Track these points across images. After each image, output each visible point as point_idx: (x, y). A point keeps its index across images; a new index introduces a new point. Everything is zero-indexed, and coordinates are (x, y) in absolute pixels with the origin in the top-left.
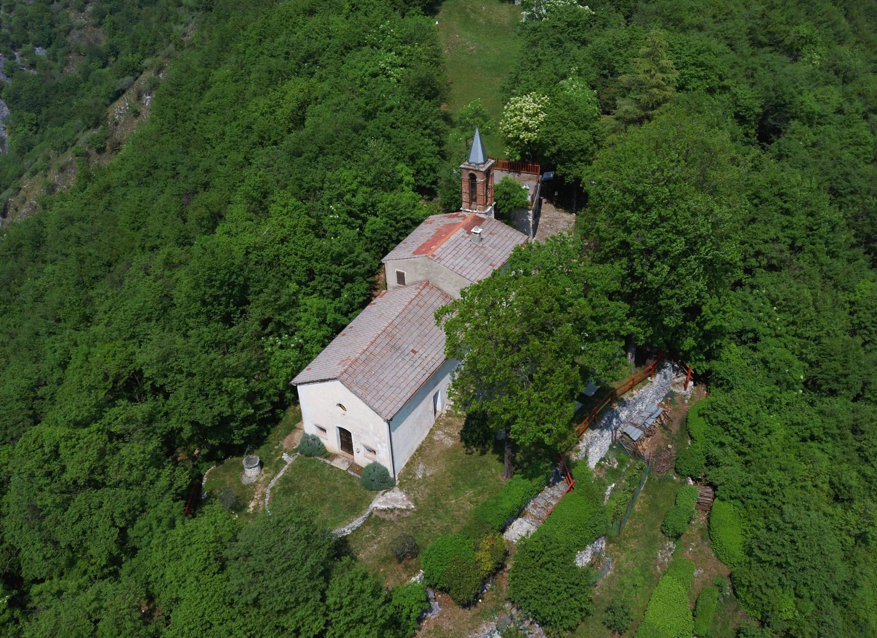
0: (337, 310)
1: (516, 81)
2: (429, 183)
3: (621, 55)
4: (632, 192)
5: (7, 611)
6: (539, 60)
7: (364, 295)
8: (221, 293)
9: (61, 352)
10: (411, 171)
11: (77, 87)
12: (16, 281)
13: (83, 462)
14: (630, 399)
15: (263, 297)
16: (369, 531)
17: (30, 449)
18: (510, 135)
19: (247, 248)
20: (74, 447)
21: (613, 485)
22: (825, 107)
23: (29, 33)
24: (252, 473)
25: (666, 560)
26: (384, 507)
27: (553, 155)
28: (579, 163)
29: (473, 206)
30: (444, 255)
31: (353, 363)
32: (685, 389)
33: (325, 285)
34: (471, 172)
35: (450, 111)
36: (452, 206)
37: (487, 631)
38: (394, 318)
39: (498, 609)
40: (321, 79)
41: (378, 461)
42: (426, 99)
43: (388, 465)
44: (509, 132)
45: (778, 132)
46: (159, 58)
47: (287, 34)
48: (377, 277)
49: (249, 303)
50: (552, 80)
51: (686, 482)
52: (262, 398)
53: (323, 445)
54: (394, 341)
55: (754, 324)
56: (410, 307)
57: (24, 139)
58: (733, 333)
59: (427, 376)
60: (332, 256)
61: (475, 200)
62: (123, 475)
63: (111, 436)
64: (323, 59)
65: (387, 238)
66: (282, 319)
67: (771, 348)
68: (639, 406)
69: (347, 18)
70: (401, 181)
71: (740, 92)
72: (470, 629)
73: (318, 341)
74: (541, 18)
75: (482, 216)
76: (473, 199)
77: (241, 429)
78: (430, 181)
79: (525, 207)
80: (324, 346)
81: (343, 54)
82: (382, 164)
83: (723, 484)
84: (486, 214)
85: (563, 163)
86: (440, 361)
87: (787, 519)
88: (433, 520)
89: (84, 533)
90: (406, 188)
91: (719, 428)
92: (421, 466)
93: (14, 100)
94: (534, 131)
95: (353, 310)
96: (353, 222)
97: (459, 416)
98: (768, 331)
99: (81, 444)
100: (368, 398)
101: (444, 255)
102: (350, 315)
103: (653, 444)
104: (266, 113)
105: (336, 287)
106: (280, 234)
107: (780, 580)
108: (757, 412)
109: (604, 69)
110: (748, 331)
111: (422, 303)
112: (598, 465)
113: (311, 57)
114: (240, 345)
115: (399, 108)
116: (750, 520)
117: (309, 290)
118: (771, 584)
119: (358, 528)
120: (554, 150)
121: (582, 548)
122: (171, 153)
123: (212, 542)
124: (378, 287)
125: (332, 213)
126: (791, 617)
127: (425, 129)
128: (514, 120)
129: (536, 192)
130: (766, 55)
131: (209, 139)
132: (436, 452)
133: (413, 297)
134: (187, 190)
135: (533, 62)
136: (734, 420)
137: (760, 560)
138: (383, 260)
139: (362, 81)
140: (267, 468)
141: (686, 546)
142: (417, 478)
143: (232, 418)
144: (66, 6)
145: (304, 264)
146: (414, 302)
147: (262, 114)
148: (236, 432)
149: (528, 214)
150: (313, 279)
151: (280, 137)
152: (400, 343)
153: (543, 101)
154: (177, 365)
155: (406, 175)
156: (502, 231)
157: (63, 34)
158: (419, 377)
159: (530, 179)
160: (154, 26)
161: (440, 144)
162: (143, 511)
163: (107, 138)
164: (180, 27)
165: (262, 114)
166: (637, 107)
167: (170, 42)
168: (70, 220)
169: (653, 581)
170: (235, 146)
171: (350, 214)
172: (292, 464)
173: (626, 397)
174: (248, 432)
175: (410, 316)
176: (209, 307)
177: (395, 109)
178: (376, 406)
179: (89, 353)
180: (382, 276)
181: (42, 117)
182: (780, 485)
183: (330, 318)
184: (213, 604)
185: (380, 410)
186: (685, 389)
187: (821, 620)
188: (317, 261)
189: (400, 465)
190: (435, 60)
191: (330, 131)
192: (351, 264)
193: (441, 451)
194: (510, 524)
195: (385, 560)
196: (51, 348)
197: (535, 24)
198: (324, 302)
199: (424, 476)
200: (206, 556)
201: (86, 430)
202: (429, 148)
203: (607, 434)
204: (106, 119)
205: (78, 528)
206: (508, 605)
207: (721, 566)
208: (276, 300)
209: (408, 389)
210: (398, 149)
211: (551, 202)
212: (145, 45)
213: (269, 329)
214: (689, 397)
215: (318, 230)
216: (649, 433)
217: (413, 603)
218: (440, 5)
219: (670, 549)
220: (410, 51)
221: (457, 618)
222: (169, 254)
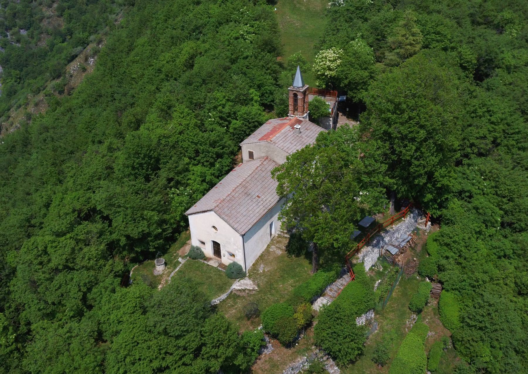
0: (213, 174)
1: (324, 42)
2: (269, 102)
3: (389, 27)
4: (391, 102)
5: (14, 344)
6: (338, 29)
7: (229, 166)
8: (143, 162)
9: (46, 197)
10: (258, 94)
11: (46, 54)
12: (12, 166)
13: (62, 255)
14: (391, 230)
15: (168, 165)
16: (230, 302)
17: (30, 249)
18: (319, 73)
19: (159, 137)
20: (56, 247)
21: (380, 281)
22: (519, 61)
23: (16, 20)
24: (160, 269)
25: (412, 325)
27: (346, 86)
28: (361, 90)
29: (295, 113)
30: (278, 141)
31: (222, 201)
32: (426, 226)
33: (205, 159)
34: (294, 92)
35: (283, 62)
36: (283, 114)
37: (301, 362)
38: (247, 177)
39: (308, 349)
40: (204, 42)
41: (236, 261)
42: (268, 52)
43: (241, 263)
44: (318, 71)
45: (487, 76)
46: (100, 35)
47: (183, 16)
48: (236, 157)
49: (160, 169)
50: (345, 40)
51: (425, 280)
52: (166, 225)
53: (203, 253)
54: (246, 190)
55: (469, 187)
56: (257, 171)
57: (11, 87)
58: (456, 193)
59: (266, 211)
60: (210, 142)
61: (297, 110)
62: (85, 263)
63: (78, 241)
64: (205, 31)
65: (243, 133)
66: (180, 179)
67: (480, 201)
68: (396, 235)
69: (220, 6)
70: (252, 99)
71: (463, 50)
72: (290, 360)
73: (201, 192)
74: (340, 6)
75: (301, 119)
76: (295, 109)
77: (153, 242)
78: (270, 100)
79: (327, 116)
80: (204, 195)
81: (217, 27)
82: (241, 89)
83: (447, 281)
84: (303, 118)
85: (351, 90)
86: (274, 203)
87: (485, 300)
88: (269, 296)
89: (62, 295)
90: (255, 104)
91: (445, 248)
92: (262, 266)
93: (6, 62)
94: (334, 70)
95: (222, 175)
96: (223, 123)
97: (286, 237)
98: (478, 191)
99: (61, 245)
100: (231, 222)
101: (278, 141)
102: (220, 178)
103: (405, 258)
104: (170, 61)
105: (212, 160)
106: (180, 128)
107: (481, 337)
108: (469, 238)
109: (378, 35)
110: (466, 192)
111: (263, 169)
112: (370, 269)
113: (197, 28)
114: (154, 192)
115: (251, 57)
116: (463, 302)
117: (196, 162)
118: (475, 339)
119: (224, 300)
120: (346, 82)
121: (360, 315)
122: (111, 87)
123: (138, 298)
124: (237, 162)
125: (210, 117)
126: (488, 360)
127: (267, 70)
128: (322, 63)
129: (334, 107)
130: (481, 29)
131: (134, 78)
132: (271, 257)
133: (258, 165)
134: (121, 108)
135: (334, 30)
136: (454, 242)
137: (468, 325)
138: (241, 145)
139: (229, 42)
140: (169, 266)
141: (424, 318)
142: (259, 272)
143: (149, 234)
144: (40, 4)
145: (193, 146)
146: (259, 168)
147: (167, 62)
148: (151, 243)
149: (330, 120)
150: (198, 156)
151: (178, 76)
152: (250, 191)
153: (339, 53)
154: (118, 203)
155: (255, 96)
156: (313, 128)
157: (38, 21)
158: (261, 211)
159: (331, 100)
160: (97, 16)
161: (276, 79)
162: (96, 284)
163: (65, 85)
164: (114, 16)
165: (167, 62)
166: (398, 58)
167: (107, 25)
168: (47, 129)
169: (402, 336)
170: (150, 81)
172: (184, 264)
173: (388, 229)
174: (158, 244)
175: (256, 176)
176: (137, 171)
177: (249, 58)
178: (235, 226)
179: (63, 198)
180: (240, 156)
181: (23, 73)
182: (483, 281)
183: (208, 178)
184: (140, 331)
185: (238, 228)
186: (426, 226)
187: (507, 362)
188: (201, 145)
189: (250, 264)
190: (274, 28)
191: (210, 70)
192: (221, 147)
193: (274, 258)
194: (316, 300)
196: (40, 196)
197: (336, 8)
198: (205, 169)
199: (264, 271)
200: (134, 305)
201: (63, 238)
202: (269, 81)
203: (376, 250)
204: (65, 73)
205: (59, 292)
206: (313, 347)
207: (446, 330)
208: (176, 167)
209: (254, 218)
210: (250, 81)
211: (345, 115)
212: (91, 27)
213: (172, 184)
214: (428, 231)
215: (201, 126)
216: (402, 251)
219: (414, 319)
220: (258, 25)
221: (282, 354)
222: (111, 143)
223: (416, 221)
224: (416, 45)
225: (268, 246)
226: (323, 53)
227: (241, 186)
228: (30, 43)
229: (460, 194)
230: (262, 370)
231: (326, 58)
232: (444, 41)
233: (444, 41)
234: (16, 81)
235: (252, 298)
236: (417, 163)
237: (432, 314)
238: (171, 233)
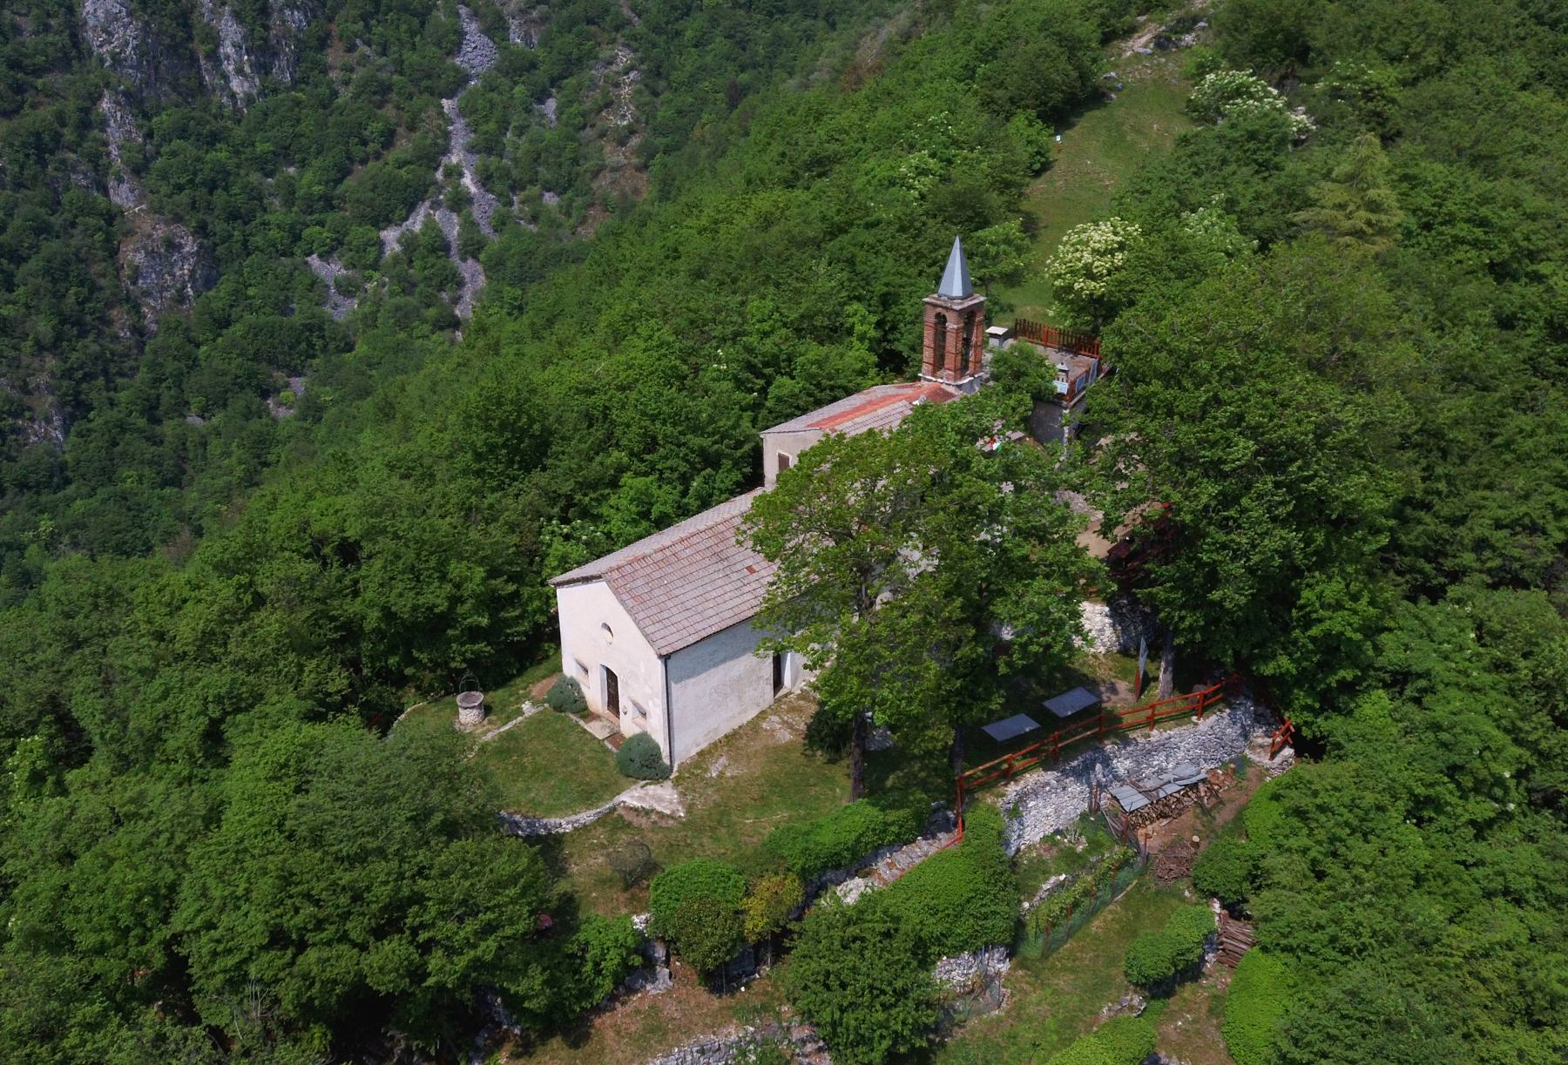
16: (601, 835)
21: (1062, 877)
23: (540, 169)
24: (468, 717)
26: (637, 804)
32: (1272, 757)
41: (649, 731)
43: (660, 738)
67: (1449, 705)
68: (1159, 760)
75: (951, 389)
84: (959, 387)
92: (723, 760)
117: (643, 468)
119: (585, 826)
132: (757, 745)
171: (750, 367)
173: (1132, 735)
195: (603, 882)
199: (721, 775)
203: (1075, 788)
209: (715, 619)
217: (609, 944)
218: (1081, 115)
219: (1131, 1008)
223: (1245, 735)
224: (1377, 238)
225: (762, 715)
226: (1084, 230)
227: (710, 533)
228: (560, 226)
229: (1398, 680)
230: (618, 1033)
231: (1087, 244)
232: (1496, 247)
233: (1496, 247)
234: (509, 314)
235: (660, 836)
236: (1222, 537)
237: (1204, 1009)
238: (525, 633)
